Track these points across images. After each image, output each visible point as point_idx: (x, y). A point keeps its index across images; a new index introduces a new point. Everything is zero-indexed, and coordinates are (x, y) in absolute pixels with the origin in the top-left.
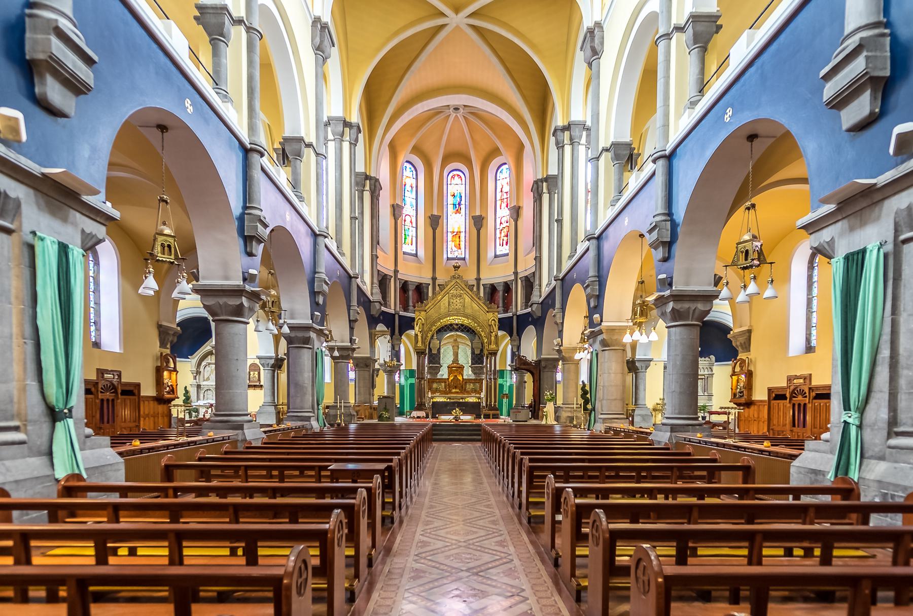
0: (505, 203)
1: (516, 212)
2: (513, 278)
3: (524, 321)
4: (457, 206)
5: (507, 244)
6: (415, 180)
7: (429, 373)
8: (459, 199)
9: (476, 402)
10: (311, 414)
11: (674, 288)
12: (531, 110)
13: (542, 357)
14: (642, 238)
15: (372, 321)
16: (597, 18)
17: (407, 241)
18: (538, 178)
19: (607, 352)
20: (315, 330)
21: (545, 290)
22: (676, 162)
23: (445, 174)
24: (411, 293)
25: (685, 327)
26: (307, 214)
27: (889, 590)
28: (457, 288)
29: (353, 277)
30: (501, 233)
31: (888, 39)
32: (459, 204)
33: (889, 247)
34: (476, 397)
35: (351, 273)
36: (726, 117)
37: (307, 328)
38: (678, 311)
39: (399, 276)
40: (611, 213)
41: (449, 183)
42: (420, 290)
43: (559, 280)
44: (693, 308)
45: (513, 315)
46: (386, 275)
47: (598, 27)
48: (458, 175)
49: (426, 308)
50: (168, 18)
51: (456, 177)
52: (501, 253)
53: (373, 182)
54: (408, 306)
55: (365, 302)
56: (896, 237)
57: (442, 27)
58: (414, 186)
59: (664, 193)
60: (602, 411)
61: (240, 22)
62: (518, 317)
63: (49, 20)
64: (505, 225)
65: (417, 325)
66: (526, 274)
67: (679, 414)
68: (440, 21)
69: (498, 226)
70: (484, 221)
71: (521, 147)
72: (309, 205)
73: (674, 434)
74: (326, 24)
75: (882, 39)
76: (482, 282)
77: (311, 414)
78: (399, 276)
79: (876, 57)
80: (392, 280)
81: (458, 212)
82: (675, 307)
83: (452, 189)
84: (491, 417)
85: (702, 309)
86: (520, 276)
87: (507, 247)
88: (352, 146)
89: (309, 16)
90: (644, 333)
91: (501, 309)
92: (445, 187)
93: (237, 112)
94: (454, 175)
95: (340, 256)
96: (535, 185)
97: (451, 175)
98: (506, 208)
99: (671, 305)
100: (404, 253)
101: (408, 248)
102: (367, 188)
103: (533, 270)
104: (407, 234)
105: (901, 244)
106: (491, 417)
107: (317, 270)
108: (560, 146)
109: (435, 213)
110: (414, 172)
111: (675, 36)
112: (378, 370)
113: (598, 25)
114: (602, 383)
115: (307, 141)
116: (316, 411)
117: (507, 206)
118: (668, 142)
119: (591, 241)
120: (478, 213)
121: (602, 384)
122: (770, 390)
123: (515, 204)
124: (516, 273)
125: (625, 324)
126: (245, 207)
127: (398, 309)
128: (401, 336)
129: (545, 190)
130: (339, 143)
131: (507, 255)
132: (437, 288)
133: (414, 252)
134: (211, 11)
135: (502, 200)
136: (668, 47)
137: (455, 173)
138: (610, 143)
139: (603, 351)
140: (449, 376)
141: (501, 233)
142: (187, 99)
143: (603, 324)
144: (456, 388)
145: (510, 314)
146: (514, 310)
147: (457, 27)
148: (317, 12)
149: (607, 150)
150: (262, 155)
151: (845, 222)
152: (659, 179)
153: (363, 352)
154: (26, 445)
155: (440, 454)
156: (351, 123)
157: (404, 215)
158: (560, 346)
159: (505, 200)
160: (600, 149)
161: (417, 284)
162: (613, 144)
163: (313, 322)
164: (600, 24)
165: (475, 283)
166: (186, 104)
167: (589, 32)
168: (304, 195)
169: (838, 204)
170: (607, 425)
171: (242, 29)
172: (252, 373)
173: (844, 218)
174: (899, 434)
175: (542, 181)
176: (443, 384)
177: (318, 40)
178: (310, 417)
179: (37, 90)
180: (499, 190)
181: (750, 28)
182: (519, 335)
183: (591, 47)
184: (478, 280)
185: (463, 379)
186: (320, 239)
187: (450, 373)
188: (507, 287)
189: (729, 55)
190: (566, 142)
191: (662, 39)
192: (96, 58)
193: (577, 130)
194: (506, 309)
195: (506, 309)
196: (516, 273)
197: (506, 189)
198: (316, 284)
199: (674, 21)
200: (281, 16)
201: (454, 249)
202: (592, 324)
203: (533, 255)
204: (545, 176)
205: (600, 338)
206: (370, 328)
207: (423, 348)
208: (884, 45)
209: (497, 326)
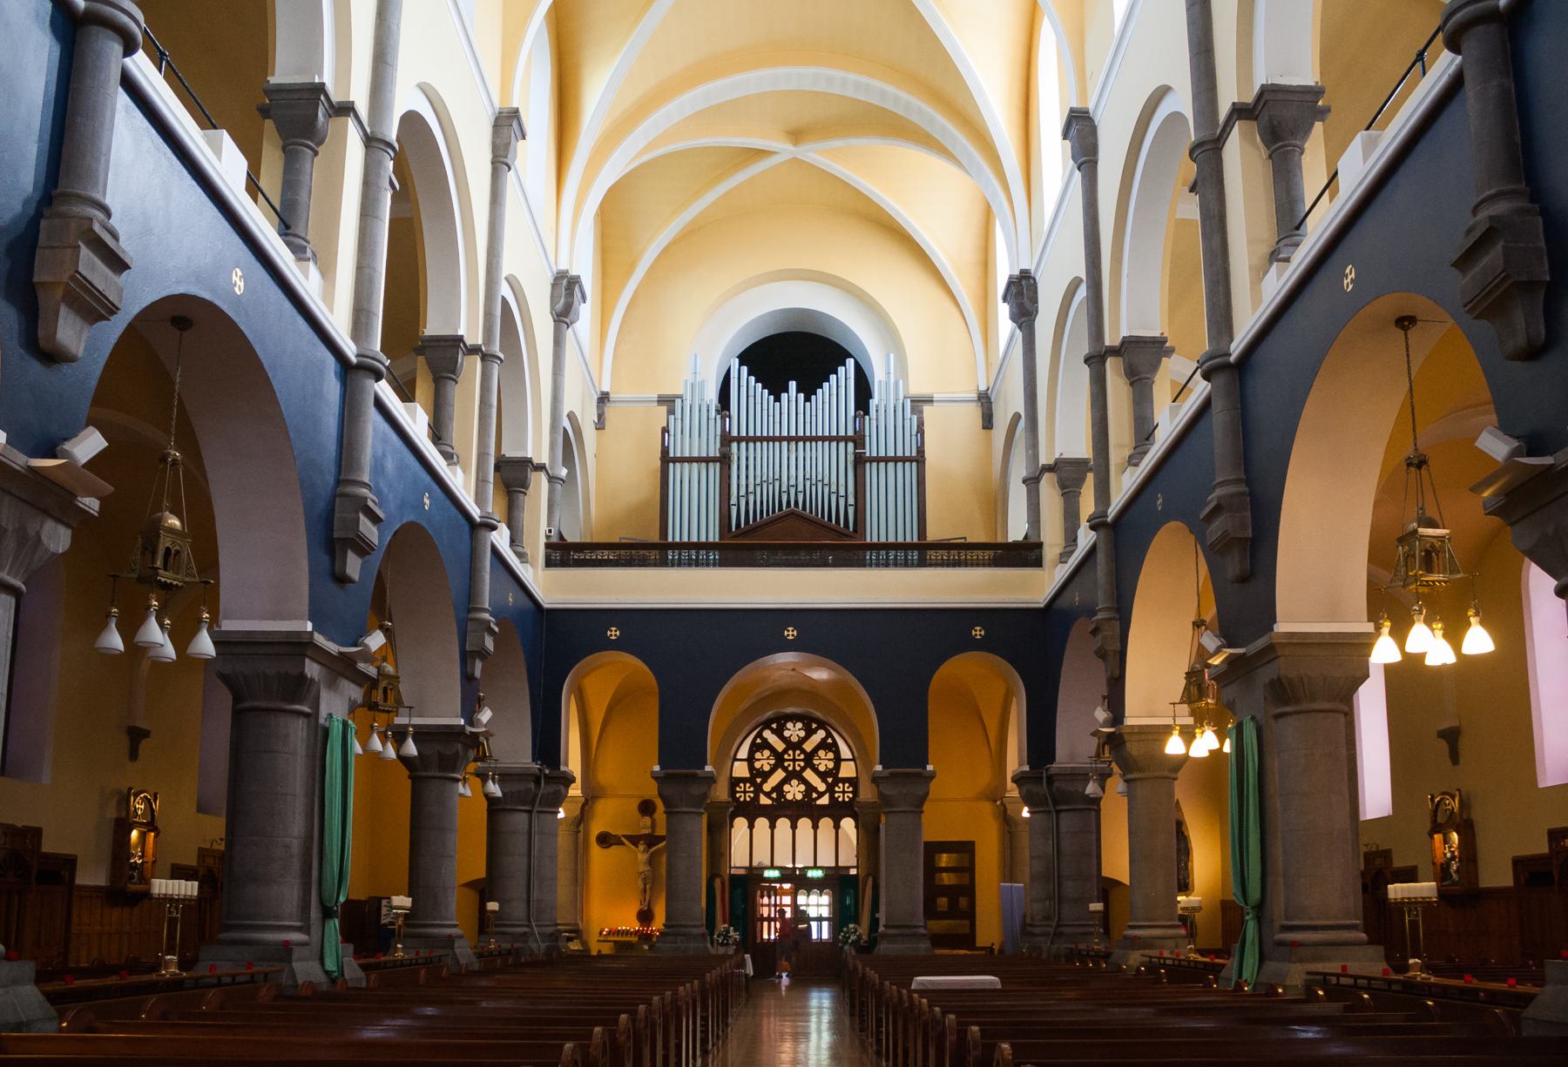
14: (1405, 329)
20: (321, 655)
27: (829, 933)
35: (476, 513)
36: (1345, 282)
37: (299, 646)
40: (1277, 284)
61: (474, 350)
72: (327, 272)
93: (464, 472)
115: (536, 461)
116: (316, 929)
118: (1108, 505)
122: (1518, 863)
126: (338, 482)
138: (1257, 88)
139: (1278, 717)
154: (309, 947)
160: (1224, 110)
166: (242, 285)
168: (527, 550)
171: (478, 359)
181: (1368, 129)
186: (483, 533)
192: (382, 515)
200: (517, 301)
205: (1266, 674)
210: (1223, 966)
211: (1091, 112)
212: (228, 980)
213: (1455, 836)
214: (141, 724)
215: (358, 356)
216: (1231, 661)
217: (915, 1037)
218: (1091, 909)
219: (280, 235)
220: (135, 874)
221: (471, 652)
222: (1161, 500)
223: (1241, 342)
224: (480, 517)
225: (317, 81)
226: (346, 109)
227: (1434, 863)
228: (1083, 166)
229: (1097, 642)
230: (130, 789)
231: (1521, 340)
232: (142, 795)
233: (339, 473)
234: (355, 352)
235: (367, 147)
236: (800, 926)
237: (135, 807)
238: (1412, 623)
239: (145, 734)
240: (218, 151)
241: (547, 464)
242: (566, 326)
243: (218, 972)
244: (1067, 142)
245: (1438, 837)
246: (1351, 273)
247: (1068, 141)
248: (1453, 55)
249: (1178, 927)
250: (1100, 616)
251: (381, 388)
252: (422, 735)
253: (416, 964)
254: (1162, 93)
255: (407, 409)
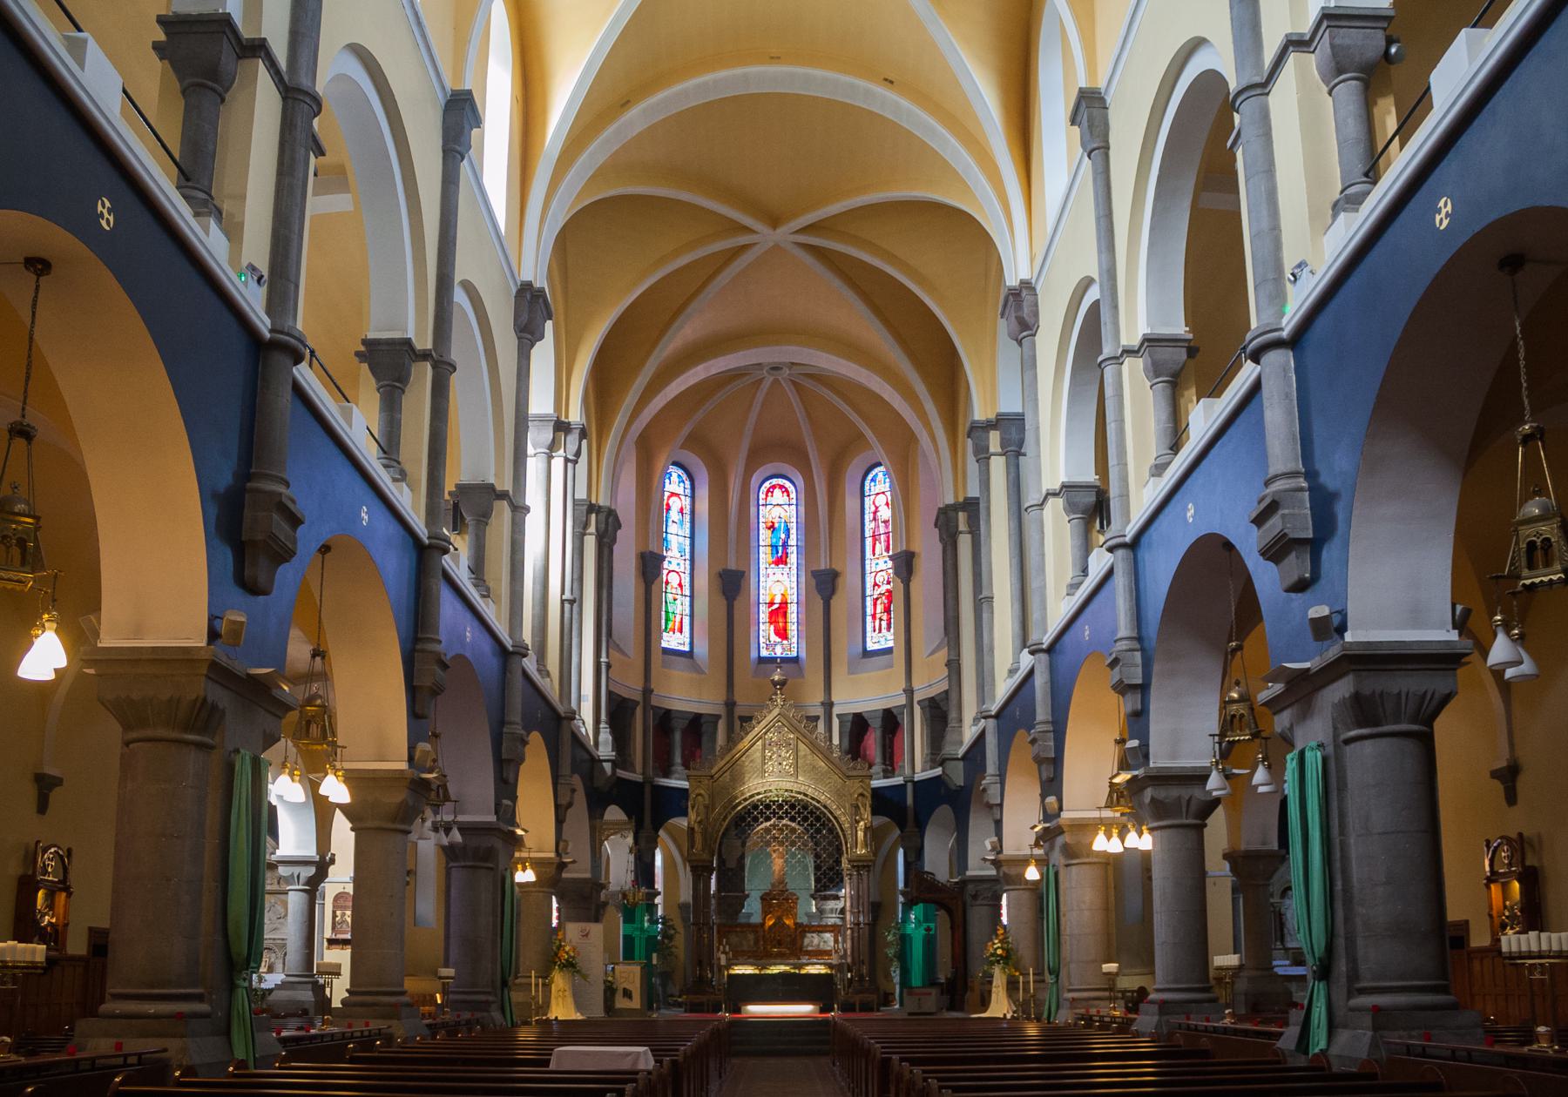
0: (883, 545)
1: (905, 564)
2: (902, 700)
3: (932, 793)
4: (780, 549)
5: (889, 629)
6: (688, 499)
7: (719, 912)
8: (783, 536)
9: (826, 975)
10: (491, 998)
11: (1152, 765)
12: (926, 377)
13: (969, 873)
15: (597, 803)
16: (1024, 274)
17: (670, 625)
18: (947, 503)
19: (1073, 867)
21: (969, 733)
22: (1145, 554)
23: (754, 482)
24: (678, 736)
25: (1181, 830)
26: (494, 620)
28: (779, 727)
29: (565, 718)
30: (875, 605)
31: (1307, 493)
32: (785, 545)
33: (1330, 749)
34: (824, 964)
36: (1438, 218)
38: (1161, 802)
39: (654, 702)
41: (761, 502)
42: (697, 726)
43: (991, 717)
44: (1187, 798)
45: (906, 782)
46: (625, 700)
47: (1027, 288)
48: (781, 487)
49: (713, 771)
50: (349, 402)
51: (777, 492)
52: (877, 647)
53: (602, 517)
54: (673, 765)
55: (587, 762)
56: (1336, 736)
57: (744, 248)
58: (687, 510)
59: (1127, 604)
60: (1070, 984)
61: (425, 356)
62: (915, 784)
63: (272, 493)
64: (884, 588)
65: (693, 808)
66: (932, 692)
67: (1176, 981)
68: (743, 240)
69: (868, 592)
70: (840, 580)
71: (910, 439)
73: (1165, 1018)
74: (542, 290)
75: (1300, 494)
76: (836, 710)
77: (491, 998)
78: (654, 702)
79: (1293, 515)
80: (639, 711)
81: (781, 561)
82: (1156, 796)
83: (768, 514)
84: (857, 1010)
85: (1203, 799)
86: (917, 697)
87: (890, 635)
88: (570, 465)
89: (438, 90)
90: (1115, 835)
91: (878, 768)
92: (753, 510)
94: (774, 487)
95: (539, 677)
96: (942, 517)
97: (767, 485)
98: (885, 554)
99: (1148, 793)
100: (666, 651)
101: (674, 640)
102: (592, 529)
103: (944, 686)
104: (670, 610)
105: (1342, 744)
106: (857, 1010)
107: (507, 719)
108: (983, 456)
109: (732, 565)
110: (688, 483)
111: (1128, 361)
112: (605, 904)
113: (1027, 285)
114: (1068, 929)
115: (499, 488)
116: (499, 992)
117: (887, 549)
118: (1129, 522)
119: (1037, 656)
120: (823, 565)
121: (1068, 932)
123: (904, 548)
124: (909, 692)
125: (1096, 814)
127: (650, 772)
128: (657, 831)
129: (962, 526)
130: (546, 460)
131: (889, 651)
132: (737, 723)
133: (687, 648)
134: (384, 348)
135: (875, 538)
136: (1120, 374)
137: (774, 481)
139: (1067, 866)
140: (764, 919)
141: (875, 605)
142: (108, 229)
143: (1064, 815)
144: (780, 944)
145: (897, 780)
146: (907, 771)
147: (777, 247)
148: (527, 275)
149: (1055, 494)
150: (298, 359)
151: (1296, 707)
152: (1120, 582)
153: (579, 871)
155: (798, 415)
156: (569, 423)
157: (665, 572)
158: (998, 854)
159: (883, 538)
160: (1044, 492)
161: (691, 716)
162: (1064, 486)
163: (498, 819)
164: (1031, 283)
165: (819, 711)
167: (1012, 294)
169: (1287, 683)
170: (1078, 1011)
172: (338, 913)
173: (1297, 701)
174: (1363, 991)
175: (955, 508)
176: (751, 937)
177: (525, 317)
178: (487, 1003)
179: (247, 572)
180: (868, 517)
182: (921, 827)
183: (1016, 317)
184: (828, 705)
185: (796, 924)
187: (765, 913)
188: (890, 720)
189: (1188, 425)
190: (992, 450)
191: (1108, 363)
193: (1014, 429)
194: (890, 769)
195: (890, 769)
196: (909, 692)
197: (885, 513)
198: (504, 744)
199: (1124, 341)
201: (774, 638)
202: (1047, 817)
203: (943, 655)
204: (961, 500)
205: (1060, 840)
206: (592, 817)
207: (705, 856)
208: (1302, 501)
209: (869, 809)
210: (1135, 1019)
211: (1103, 91)
212: (359, 1034)
213: (1516, 885)
214: (50, 770)
215: (429, 538)
216: (1045, 829)
217: (873, 1072)
218: (1104, 971)
219: (177, 188)
220: (1227, 1020)
221: (505, 760)
222: (1189, 514)
223: (1136, 523)
224: (512, 646)
225: (221, 11)
226: (258, 48)
227: (1491, 916)
228: (1093, 154)
229: (1115, 675)
230: (38, 842)
231: (1295, 578)
232: (52, 850)
233: (416, 632)
234: (427, 535)
235: (284, 99)
236: (439, 1002)
237: (44, 863)
238: (1029, 865)
239: (57, 782)
240: (207, 231)
241: (511, 492)
242: (459, 157)
243: (126, 1050)
244: (1076, 129)
245: (1495, 889)
246: (1445, 206)
247: (1076, 127)
248: (1254, 365)
249: (489, 993)
250: (1039, 728)
251: (300, 372)
252: (465, 829)
253: (344, 1038)
254: (1196, 45)
255: (484, 602)
